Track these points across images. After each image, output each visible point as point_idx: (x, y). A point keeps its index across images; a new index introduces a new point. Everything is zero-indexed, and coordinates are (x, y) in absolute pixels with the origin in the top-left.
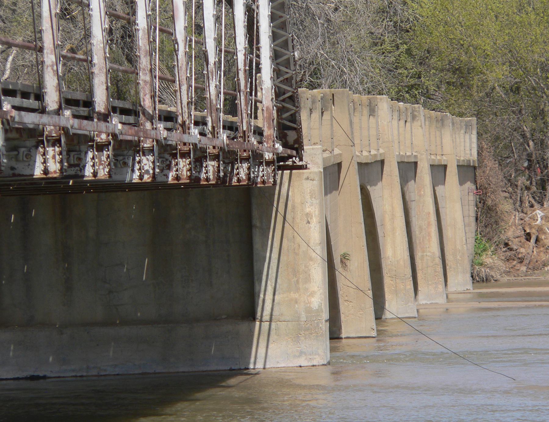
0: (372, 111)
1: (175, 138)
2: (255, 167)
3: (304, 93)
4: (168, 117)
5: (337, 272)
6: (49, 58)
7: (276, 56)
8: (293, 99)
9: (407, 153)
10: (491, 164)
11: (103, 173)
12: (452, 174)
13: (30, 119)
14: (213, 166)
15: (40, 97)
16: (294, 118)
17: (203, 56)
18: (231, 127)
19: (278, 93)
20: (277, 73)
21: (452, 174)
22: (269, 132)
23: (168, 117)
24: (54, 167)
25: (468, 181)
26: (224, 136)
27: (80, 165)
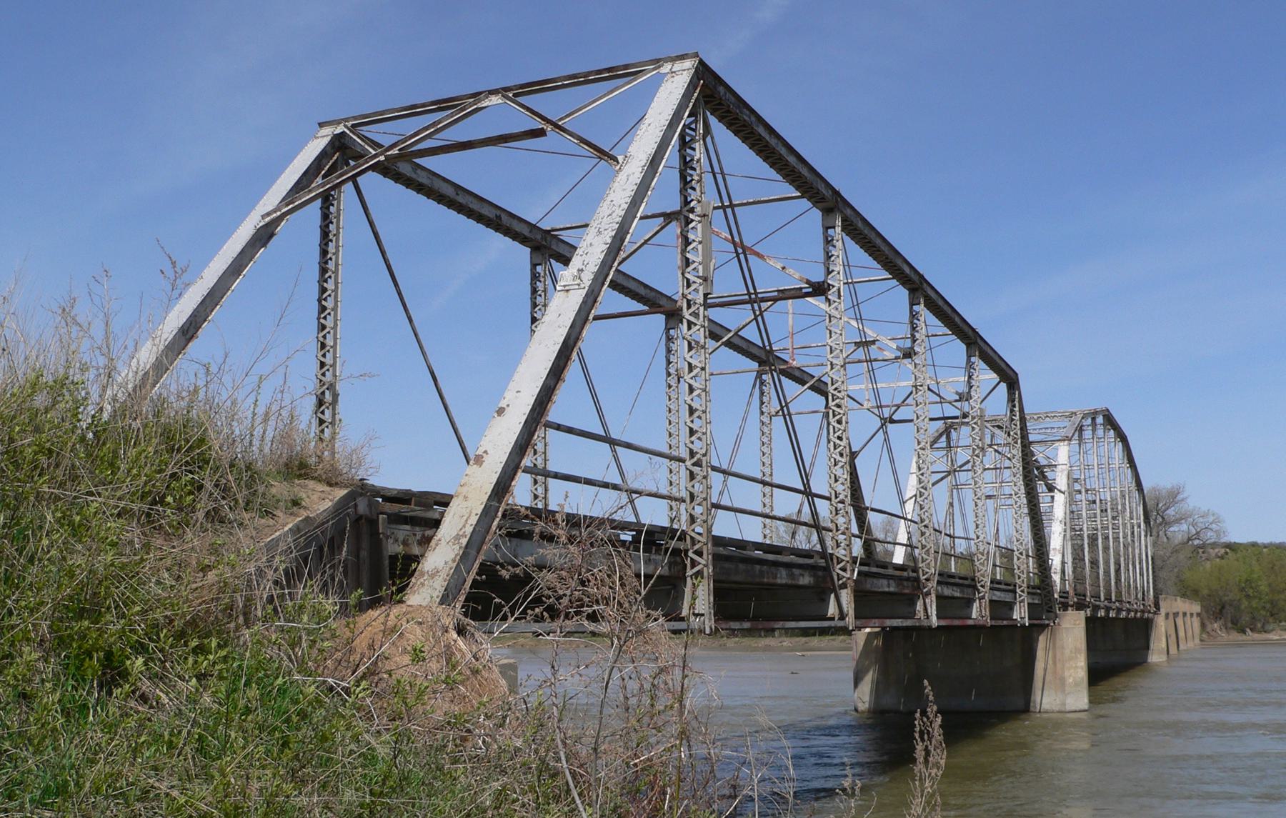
0: (1176, 600)
1: (1130, 607)
2: (910, 556)
3: (1160, 596)
4: (1129, 602)
5: (940, 323)
6: (1102, 589)
7: (1154, 588)
8: (1158, 598)
9: (1185, 611)
10: (1204, 613)
11: (1114, 616)
12: (1195, 615)
13: (1097, 603)
14: (781, 578)
15: (1099, 598)
16: (1158, 602)
17: (1137, 588)
18: (1143, 604)
19: (1154, 597)
20: (1154, 592)
21: (1195, 615)
22: (1152, 605)
23: (1129, 602)
24: (1103, 614)
25: (509, 580)
26: (1142, 607)
27: (1109, 614)
